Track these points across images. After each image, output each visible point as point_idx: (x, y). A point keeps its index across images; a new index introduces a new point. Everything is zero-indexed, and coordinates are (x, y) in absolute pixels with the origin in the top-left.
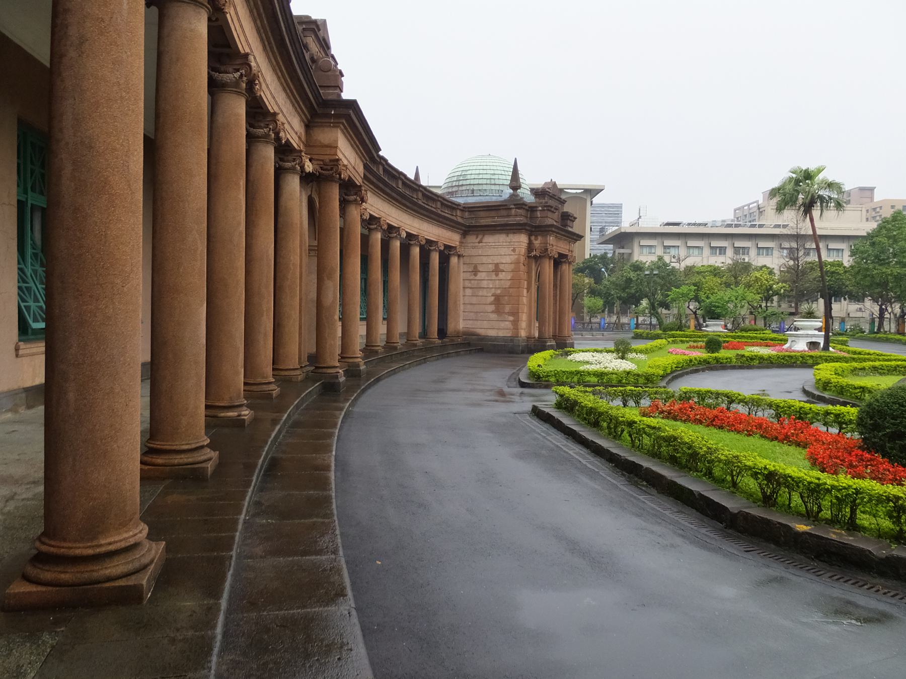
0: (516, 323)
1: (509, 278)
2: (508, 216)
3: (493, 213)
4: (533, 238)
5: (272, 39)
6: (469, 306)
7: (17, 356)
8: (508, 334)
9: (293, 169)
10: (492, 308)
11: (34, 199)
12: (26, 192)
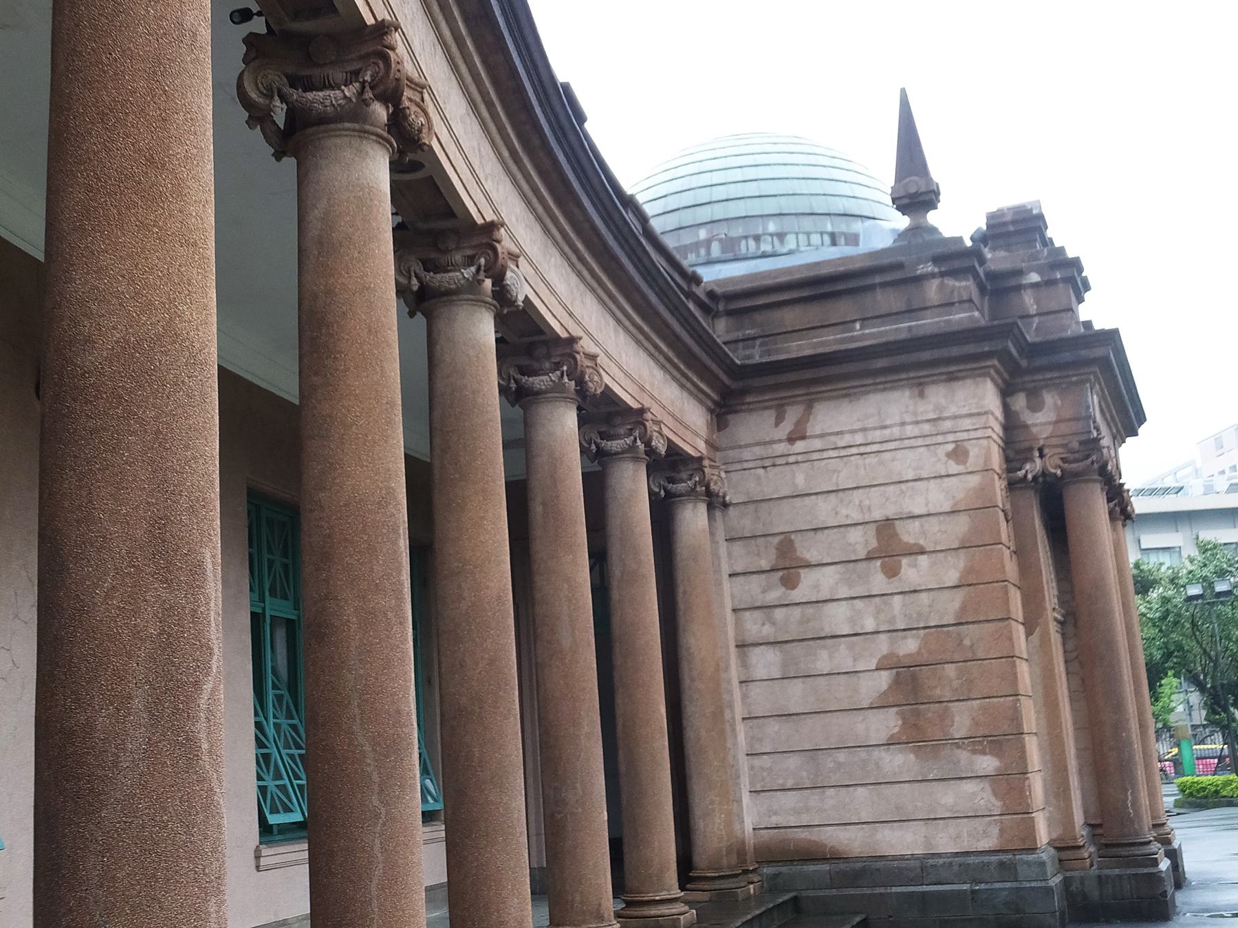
0: (1010, 784)
1: (952, 577)
2: (911, 311)
4: (1019, 402)
5: (690, 374)
6: (773, 727)
7: (258, 867)
8: (983, 838)
10: (887, 723)
11: (276, 608)
12: (262, 600)
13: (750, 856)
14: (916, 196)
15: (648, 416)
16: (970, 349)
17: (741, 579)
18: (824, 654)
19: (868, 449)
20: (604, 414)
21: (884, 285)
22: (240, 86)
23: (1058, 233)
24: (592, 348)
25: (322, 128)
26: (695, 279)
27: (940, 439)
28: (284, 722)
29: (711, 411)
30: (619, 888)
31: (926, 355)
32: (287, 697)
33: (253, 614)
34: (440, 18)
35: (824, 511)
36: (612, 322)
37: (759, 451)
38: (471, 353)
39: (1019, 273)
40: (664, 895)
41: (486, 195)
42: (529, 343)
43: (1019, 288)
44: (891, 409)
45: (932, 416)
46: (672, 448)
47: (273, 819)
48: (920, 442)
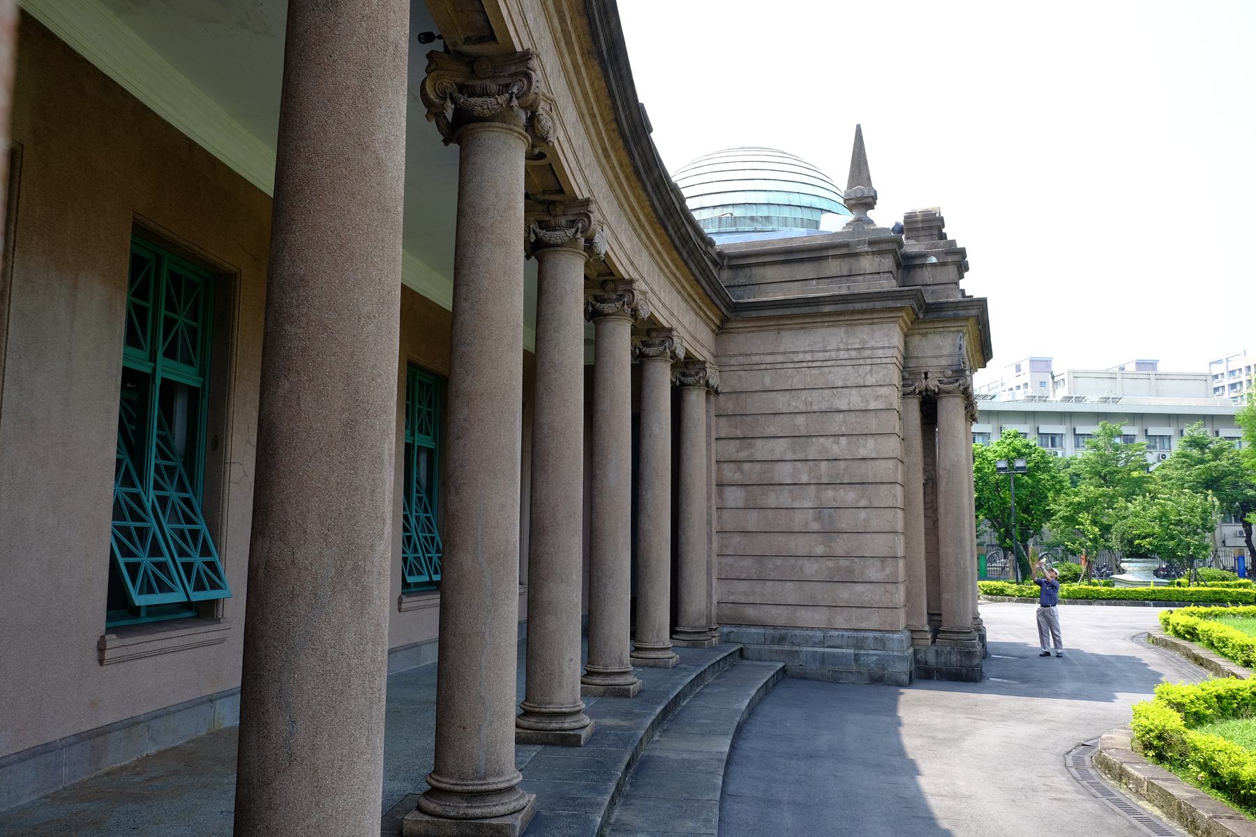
3: (807, 270)
6: (737, 539)
7: (101, 661)
9: (696, 384)
11: (423, 441)
12: (413, 435)
13: (714, 619)
14: (862, 201)
15: (675, 333)
16: (890, 304)
17: (723, 442)
18: (773, 495)
19: (814, 364)
20: (650, 334)
21: (834, 257)
22: (423, 89)
23: (950, 231)
24: (644, 287)
25: (480, 124)
26: (711, 243)
27: (862, 362)
28: (422, 515)
29: (713, 331)
30: (633, 635)
31: (858, 306)
32: (425, 499)
33: (407, 444)
34: (565, 51)
35: (781, 402)
36: (657, 269)
37: (742, 359)
38: (568, 287)
39: (924, 256)
40: (660, 645)
41: (585, 178)
42: (606, 286)
43: (923, 266)
44: (831, 340)
45: (858, 346)
46: (689, 356)
47: (410, 580)
48: (848, 362)
